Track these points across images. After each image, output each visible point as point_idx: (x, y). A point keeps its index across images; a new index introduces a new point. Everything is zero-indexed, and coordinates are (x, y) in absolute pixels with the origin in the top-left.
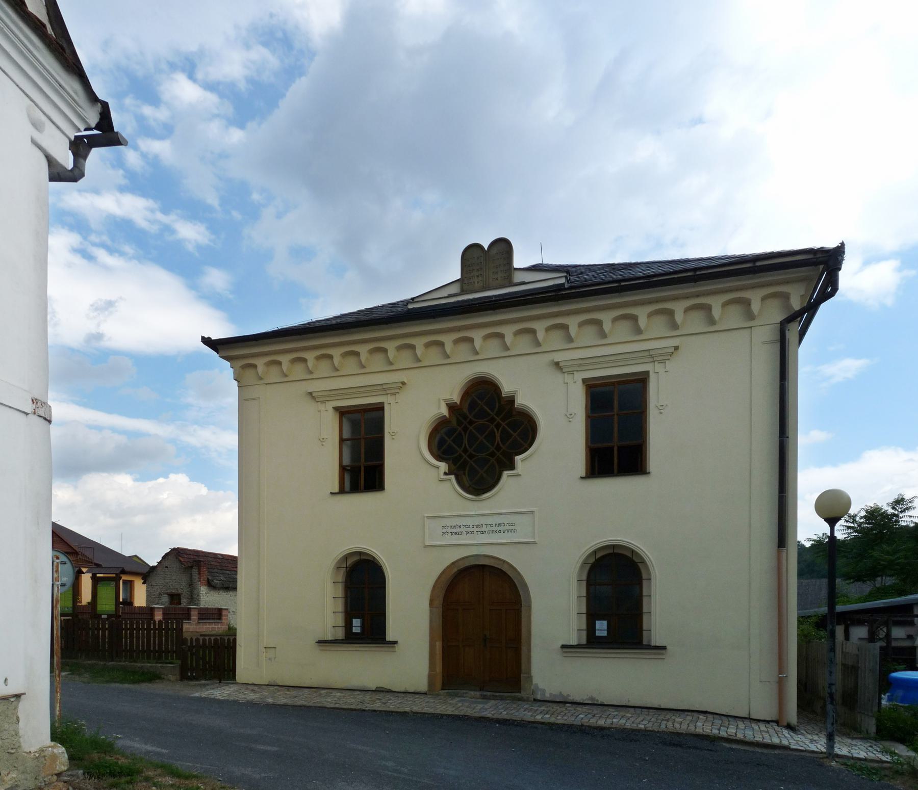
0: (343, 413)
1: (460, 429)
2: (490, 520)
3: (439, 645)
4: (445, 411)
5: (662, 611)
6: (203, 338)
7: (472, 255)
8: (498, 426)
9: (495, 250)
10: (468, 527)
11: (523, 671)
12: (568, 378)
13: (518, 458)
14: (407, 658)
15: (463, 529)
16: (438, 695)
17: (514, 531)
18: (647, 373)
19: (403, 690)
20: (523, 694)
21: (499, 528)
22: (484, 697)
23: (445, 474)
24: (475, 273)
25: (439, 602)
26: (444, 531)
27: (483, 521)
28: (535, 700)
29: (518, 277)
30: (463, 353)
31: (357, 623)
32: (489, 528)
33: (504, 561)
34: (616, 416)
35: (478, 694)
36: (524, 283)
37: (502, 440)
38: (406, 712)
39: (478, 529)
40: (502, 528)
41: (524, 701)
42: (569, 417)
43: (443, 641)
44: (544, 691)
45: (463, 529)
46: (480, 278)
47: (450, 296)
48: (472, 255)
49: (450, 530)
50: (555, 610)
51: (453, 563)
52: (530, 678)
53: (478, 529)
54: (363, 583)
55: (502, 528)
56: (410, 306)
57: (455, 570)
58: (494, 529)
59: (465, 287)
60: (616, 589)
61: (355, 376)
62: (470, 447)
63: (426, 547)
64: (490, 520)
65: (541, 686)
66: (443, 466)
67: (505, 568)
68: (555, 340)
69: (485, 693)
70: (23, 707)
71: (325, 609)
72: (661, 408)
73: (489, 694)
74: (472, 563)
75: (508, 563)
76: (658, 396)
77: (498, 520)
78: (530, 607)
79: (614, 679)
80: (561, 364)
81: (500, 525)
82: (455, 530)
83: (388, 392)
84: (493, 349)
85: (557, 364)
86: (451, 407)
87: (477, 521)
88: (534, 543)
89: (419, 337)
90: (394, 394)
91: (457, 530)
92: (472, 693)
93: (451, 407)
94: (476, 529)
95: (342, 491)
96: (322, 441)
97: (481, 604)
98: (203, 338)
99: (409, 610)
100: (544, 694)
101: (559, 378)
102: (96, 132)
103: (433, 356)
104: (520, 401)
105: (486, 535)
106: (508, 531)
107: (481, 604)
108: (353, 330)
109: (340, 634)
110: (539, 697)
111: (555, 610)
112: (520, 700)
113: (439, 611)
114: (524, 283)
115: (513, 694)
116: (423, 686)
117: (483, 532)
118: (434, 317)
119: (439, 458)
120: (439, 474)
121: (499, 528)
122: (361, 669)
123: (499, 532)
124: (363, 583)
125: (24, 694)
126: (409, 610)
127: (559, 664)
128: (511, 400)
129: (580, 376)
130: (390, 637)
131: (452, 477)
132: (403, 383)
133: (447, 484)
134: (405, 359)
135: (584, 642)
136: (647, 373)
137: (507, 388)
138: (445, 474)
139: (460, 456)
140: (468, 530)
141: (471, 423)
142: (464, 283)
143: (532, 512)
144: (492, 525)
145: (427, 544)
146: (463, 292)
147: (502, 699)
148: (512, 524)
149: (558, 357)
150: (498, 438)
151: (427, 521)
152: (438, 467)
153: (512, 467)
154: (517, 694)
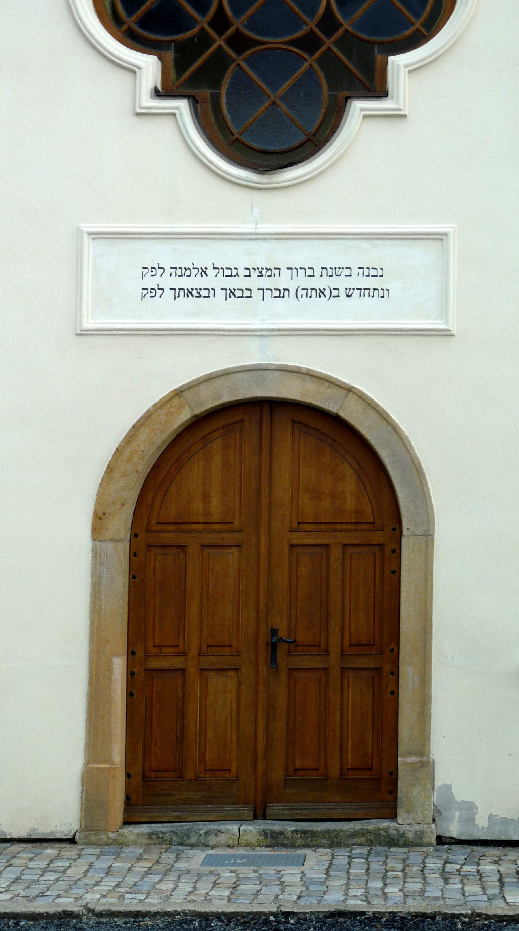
3: (119, 666)
10: (231, 273)
11: (402, 747)
13: (399, 63)
16: (119, 845)
17: (382, 293)
19: (23, 834)
20: (405, 823)
21: (334, 282)
22: (275, 840)
23: (157, 94)
25: (121, 523)
26: (150, 282)
28: (441, 840)
33: (350, 390)
35: (252, 829)
38: (67, 915)
39: (266, 282)
40: (342, 283)
41: (408, 844)
43: (131, 653)
44: (470, 808)
45: (212, 281)
49: (168, 281)
51: (179, 393)
52: (426, 767)
53: (266, 282)
55: (342, 283)
57: (185, 416)
58: (318, 283)
62: (237, 12)
63: (83, 334)
65: (461, 794)
66: (149, 67)
67: (351, 413)
69: (276, 826)
73: (290, 827)
74: (226, 398)
75: (361, 397)
78: (428, 537)
81: (335, 272)
82: (186, 283)
87: (261, 255)
92: (233, 827)
94: (255, 282)
100: (470, 820)
105: (289, 301)
106: (363, 291)
110: (454, 830)
112: (393, 842)
113: (119, 554)
115: (372, 825)
116: (63, 813)
117: (281, 294)
120: (135, 96)
121: (334, 282)
123: (334, 294)
131: (182, 107)
133: (165, 127)
139: (203, 41)
140: (232, 283)
143: (440, 237)
145: (89, 323)
147: (334, 842)
148: (376, 272)
151: (90, 248)
152: (132, 71)
153: (378, 89)
154: (385, 824)
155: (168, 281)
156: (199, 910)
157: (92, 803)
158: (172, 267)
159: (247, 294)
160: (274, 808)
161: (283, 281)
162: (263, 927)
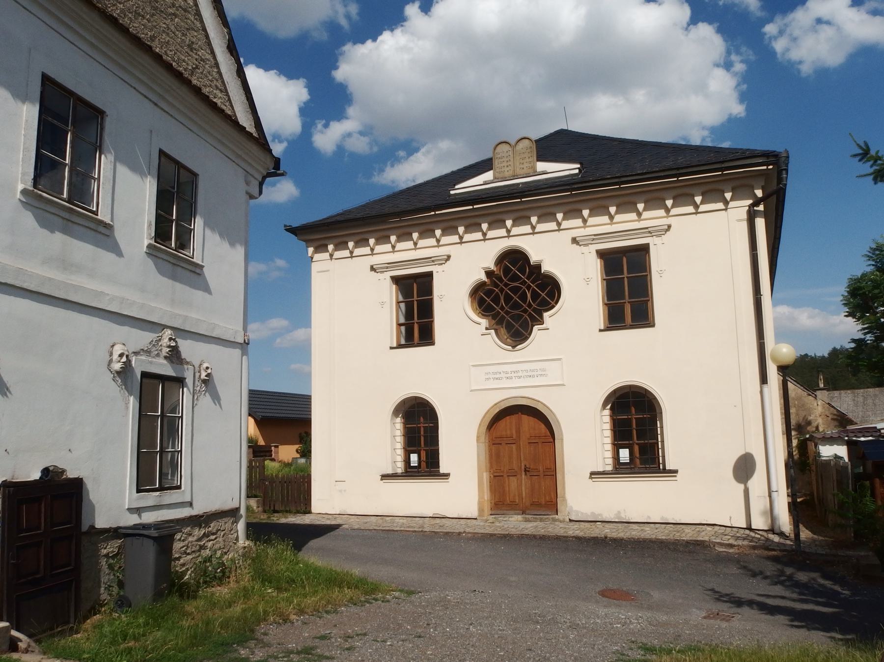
0: (396, 280)
4: (484, 277)
5: (675, 438)
6: (285, 226)
12: (584, 249)
14: (459, 493)
15: (503, 375)
18: (648, 245)
20: (560, 516)
23: (487, 329)
24: (505, 164)
31: (414, 458)
34: (626, 279)
40: (535, 373)
42: (587, 281)
45: (503, 375)
47: (485, 183)
49: (491, 376)
50: (585, 440)
54: (419, 423)
55: (535, 373)
60: (635, 420)
61: (408, 252)
65: (575, 508)
66: (484, 322)
67: (540, 407)
70: (190, 509)
71: (388, 443)
72: (660, 273)
76: (657, 261)
78: (562, 440)
79: (639, 502)
81: (533, 371)
88: (563, 385)
90: (659, 236)
91: (498, 376)
93: (489, 274)
94: (513, 375)
95: (400, 346)
96: (383, 303)
97: (521, 436)
98: (285, 226)
99: (461, 444)
104: (545, 268)
107: (521, 436)
108: (662, 534)
109: (400, 468)
111: (585, 440)
117: (520, 377)
122: (418, 500)
124: (419, 423)
125: (601, 330)
126: (461, 444)
127: (592, 492)
128: (538, 267)
129: (594, 248)
130: (443, 470)
131: (493, 331)
135: (609, 468)
136: (648, 245)
137: (534, 258)
141: (506, 285)
144: (527, 371)
150: (529, 295)
151: (473, 369)
155: (491, 376)
156: (339, 569)
157: (481, 510)
158: (295, 224)
159: (511, 378)
160: (528, 512)
161: (520, 374)
162: (244, 610)
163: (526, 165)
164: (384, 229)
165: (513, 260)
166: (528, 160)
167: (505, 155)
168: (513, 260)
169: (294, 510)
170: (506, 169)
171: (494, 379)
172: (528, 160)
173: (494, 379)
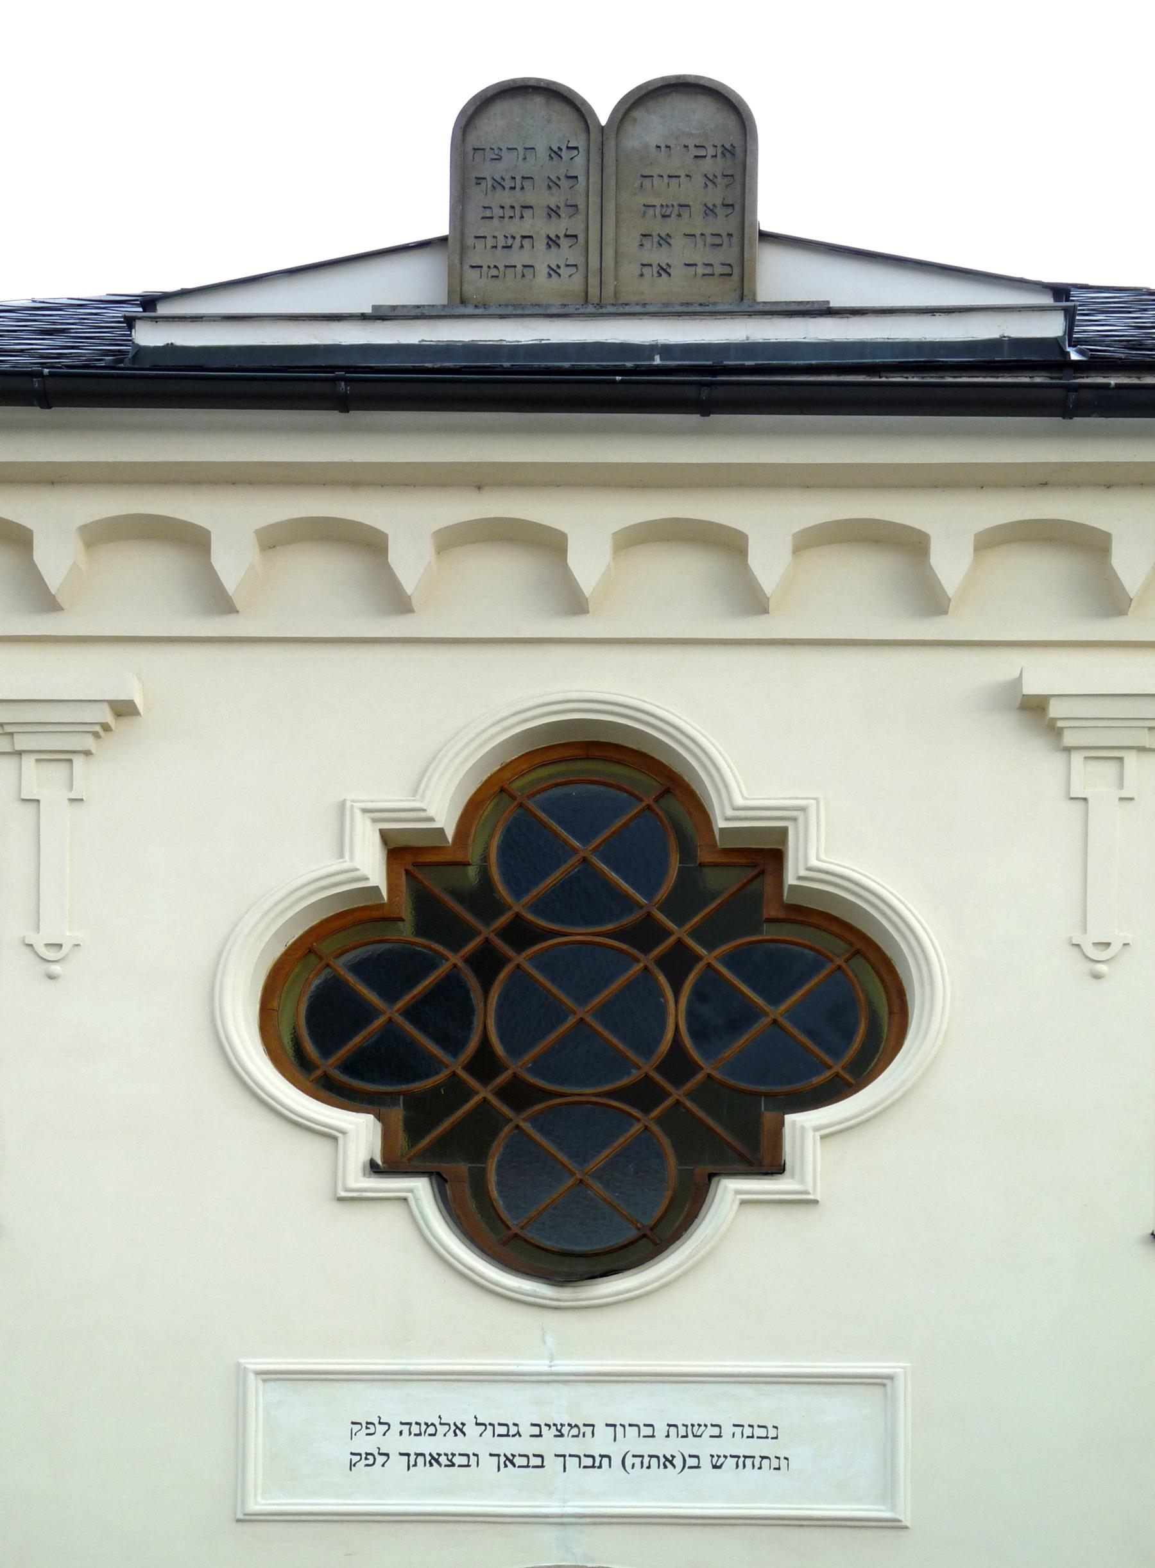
1: (677, 1094)
2: (633, 1405)
4: (369, 867)
7: (514, 134)
8: (677, 963)
9: (652, 129)
10: (509, 1431)
13: (803, 1127)
17: (779, 1464)
21: (690, 1446)
23: (374, 1169)
26: (364, 1444)
27: (594, 1405)
29: (780, 277)
30: (493, 593)
32: (633, 1443)
36: (826, 311)
37: (699, 1032)
39: (568, 1445)
40: (706, 1447)
46: (567, 253)
47: (380, 315)
48: (514, 134)
53: (568, 1445)
55: (706, 1447)
56: (148, 336)
58: (662, 1446)
59: (475, 284)
62: (515, 1050)
64: (633, 1405)
66: (361, 1132)
68: (1028, 596)
77: (687, 1406)
80: (1055, 710)
81: (692, 1431)
82: (427, 1445)
83: (21, 743)
84: (675, 591)
85: (1034, 710)
86: (405, 852)
87: (560, 1406)
88: (894, 1525)
89: (241, 486)
90: (66, 757)
91: (443, 1444)
93: (405, 852)
94: (549, 1445)
101: (1036, 767)
102: (492, 1165)
103: (317, 591)
105: (610, 1475)
106: (742, 1460)
114: (826, 311)
117: (596, 1462)
118: (344, 404)
119: (331, 1090)
121: (690, 1446)
123: (692, 1463)
128: (764, 854)
131: (420, 1189)
132: (124, 710)
134: (140, 593)
137: (741, 787)
138: (374, 1169)
139: (456, 1092)
142: (464, 255)
143: (881, 1382)
145: (259, 1504)
146: (459, 304)
148: (769, 1432)
149: (1042, 675)
151: (259, 1395)
152: (331, 1137)
161: (600, 1443)
163: (679, 254)
164: (746, 819)
165: (593, 821)
166: (698, 225)
167: (539, 166)
168: (593, 821)
169: (327, 947)
170: (542, 258)
171: (411, 1459)
172: (698, 225)
173: (411, 1459)
